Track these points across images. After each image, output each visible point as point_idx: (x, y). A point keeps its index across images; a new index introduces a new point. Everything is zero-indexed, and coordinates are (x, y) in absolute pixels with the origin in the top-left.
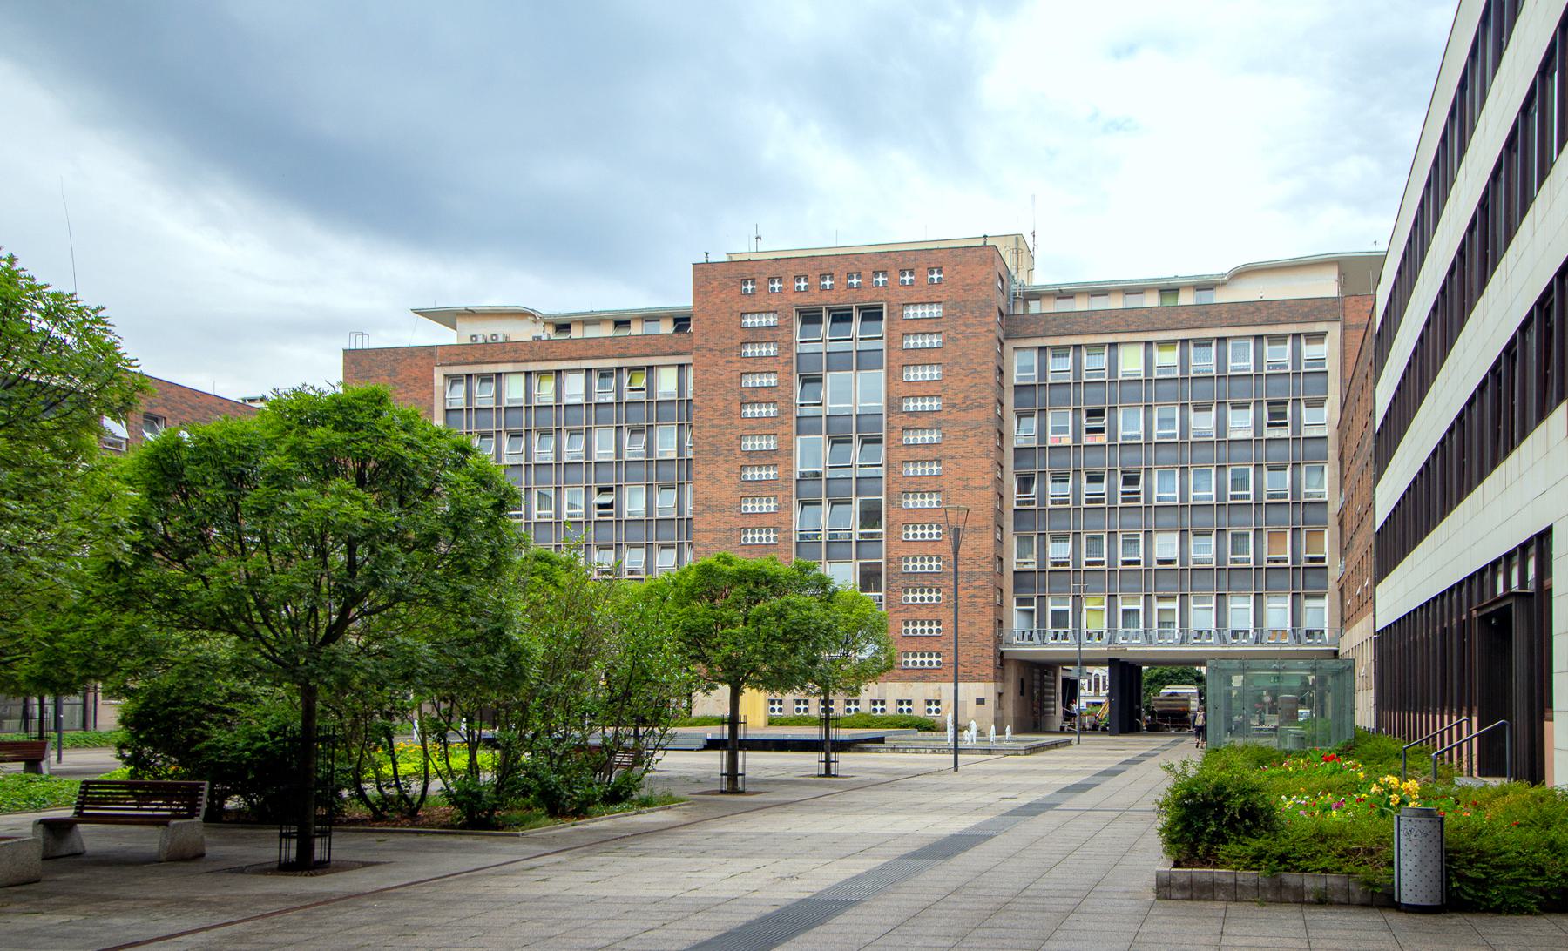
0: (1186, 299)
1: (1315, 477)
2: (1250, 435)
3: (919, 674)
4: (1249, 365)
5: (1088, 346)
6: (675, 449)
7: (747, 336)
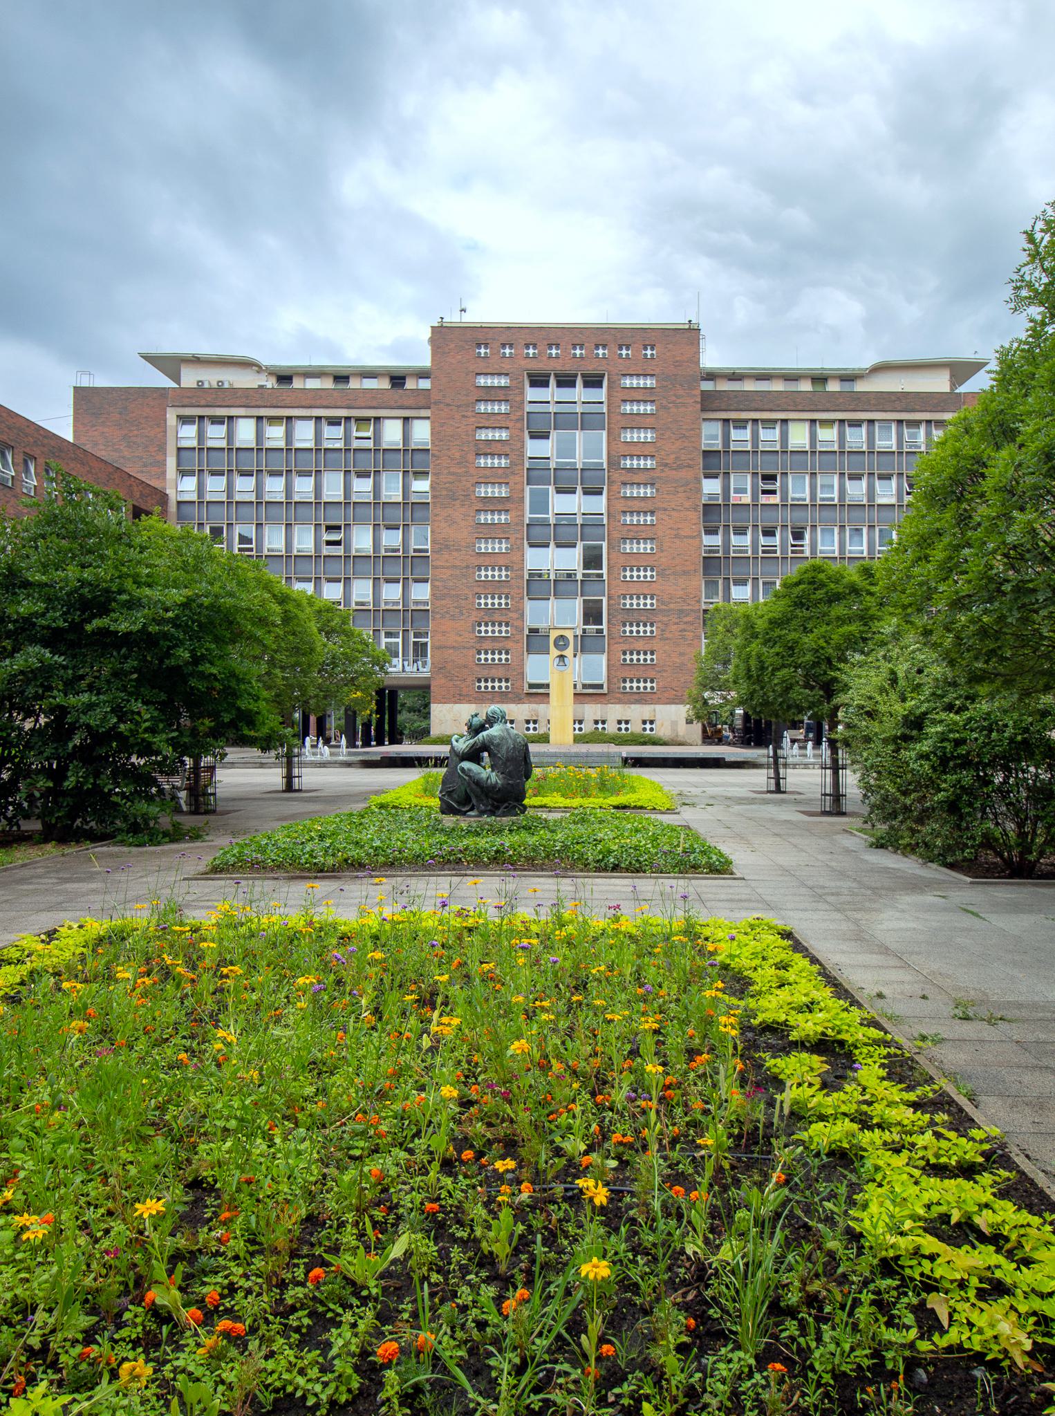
0: (833, 386)
1: (827, 537)
2: (893, 501)
3: (636, 697)
4: (892, 444)
5: (763, 421)
6: (401, 493)
7: (483, 395)
